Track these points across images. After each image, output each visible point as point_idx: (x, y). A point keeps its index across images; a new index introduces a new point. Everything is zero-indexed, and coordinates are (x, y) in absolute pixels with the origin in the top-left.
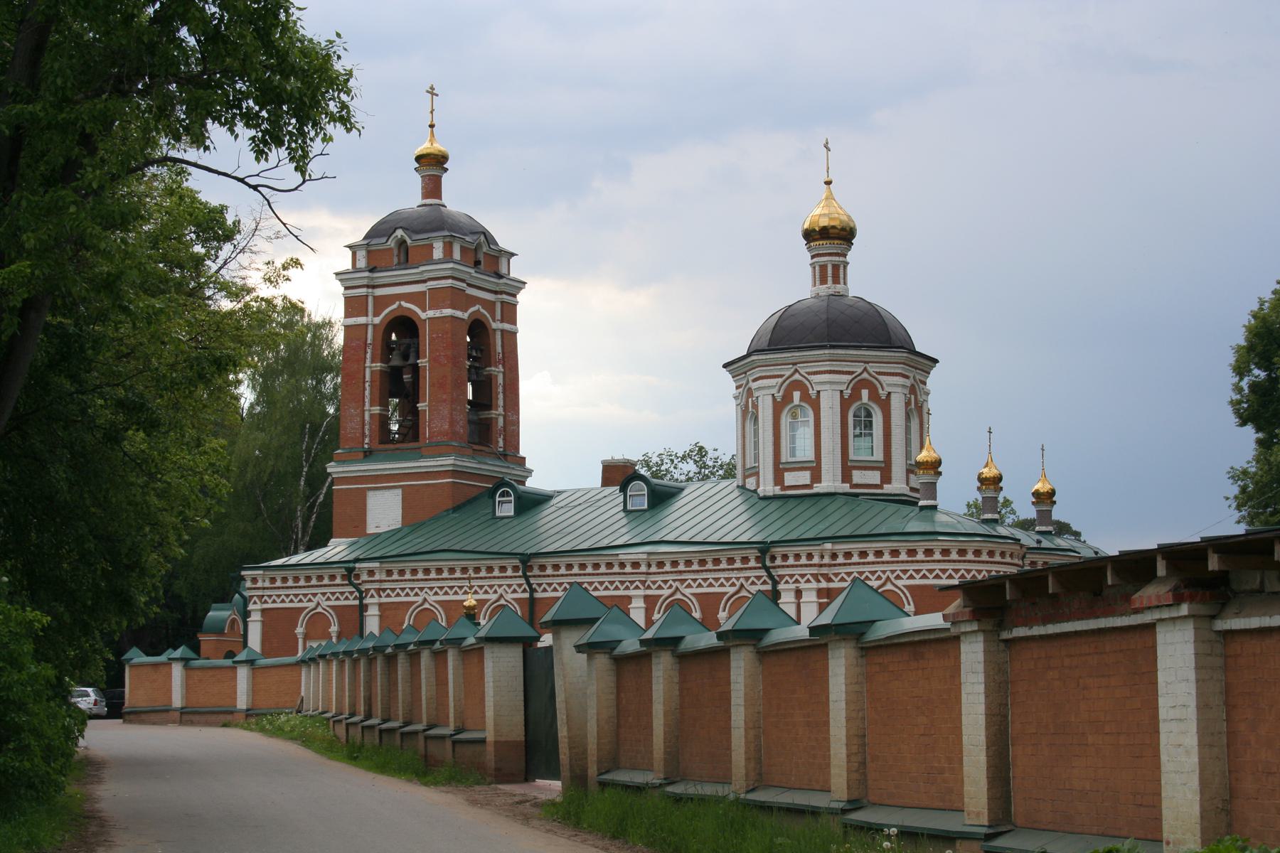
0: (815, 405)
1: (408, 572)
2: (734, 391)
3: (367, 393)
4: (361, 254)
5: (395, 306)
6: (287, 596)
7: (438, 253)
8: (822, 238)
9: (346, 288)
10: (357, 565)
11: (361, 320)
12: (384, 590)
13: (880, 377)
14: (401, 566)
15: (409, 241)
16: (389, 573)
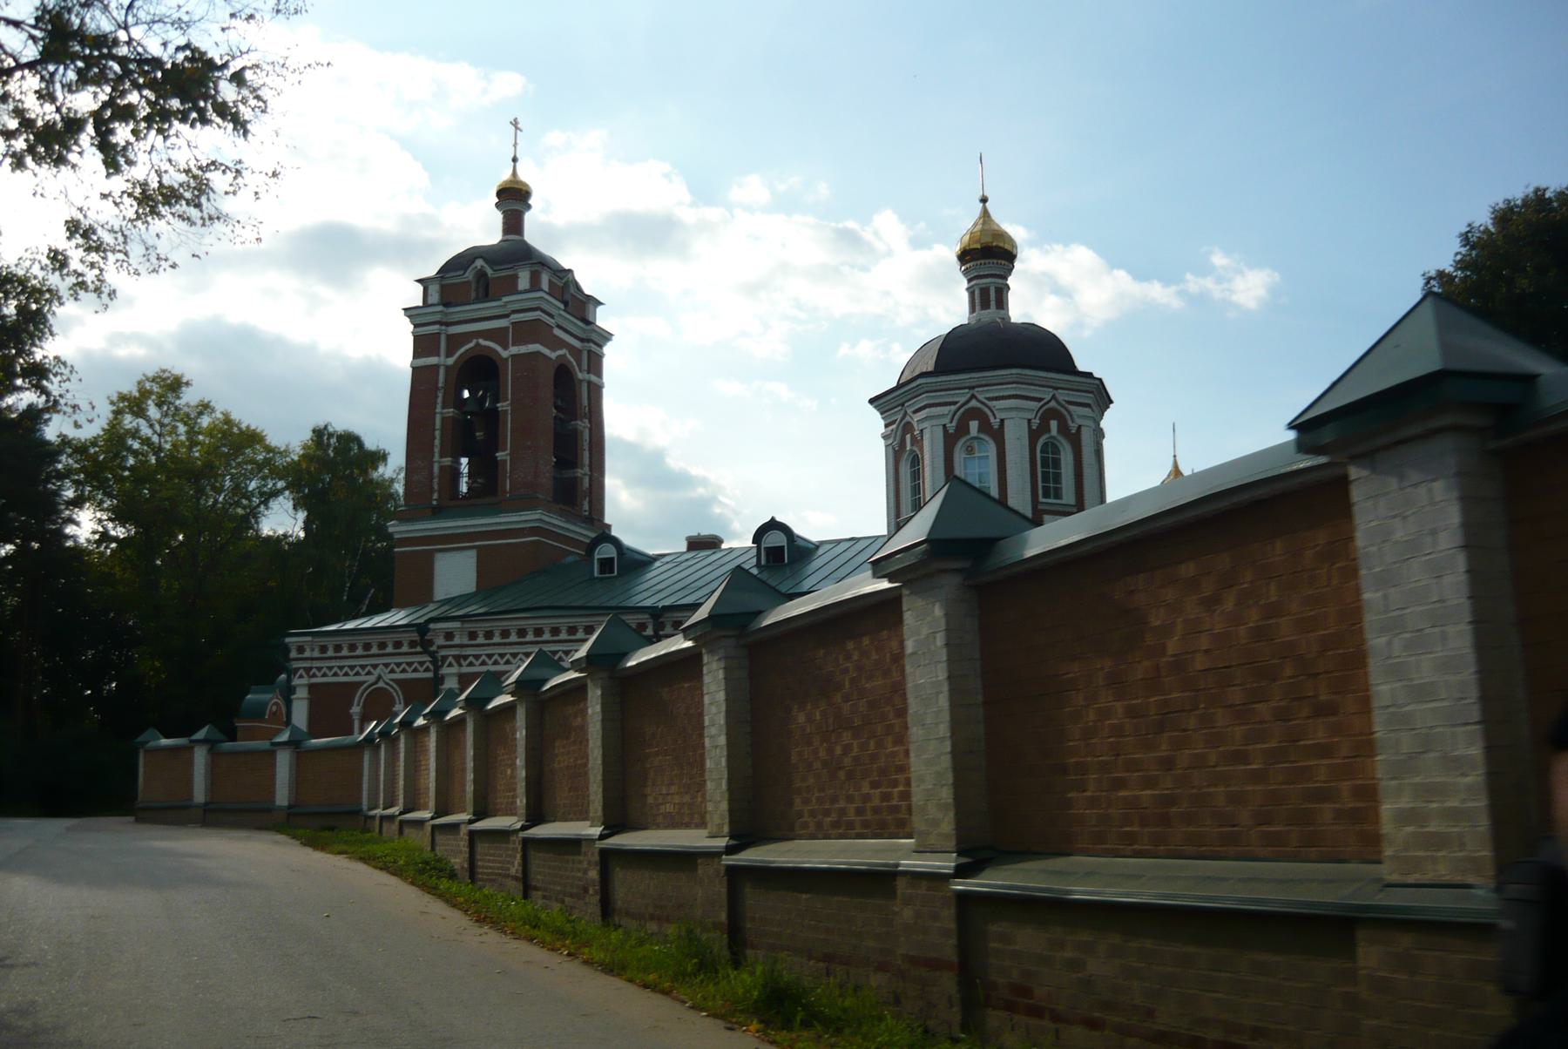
0: (998, 436)
1: (497, 634)
2: (883, 430)
3: (437, 442)
4: (434, 290)
5: (471, 345)
7: (524, 282)
8: (984, 257)
10: (432, 626)
11: (433, 360)
12: (465, 657)
13: (1071, 408)
15: (489, 272)
16: (473, 635)
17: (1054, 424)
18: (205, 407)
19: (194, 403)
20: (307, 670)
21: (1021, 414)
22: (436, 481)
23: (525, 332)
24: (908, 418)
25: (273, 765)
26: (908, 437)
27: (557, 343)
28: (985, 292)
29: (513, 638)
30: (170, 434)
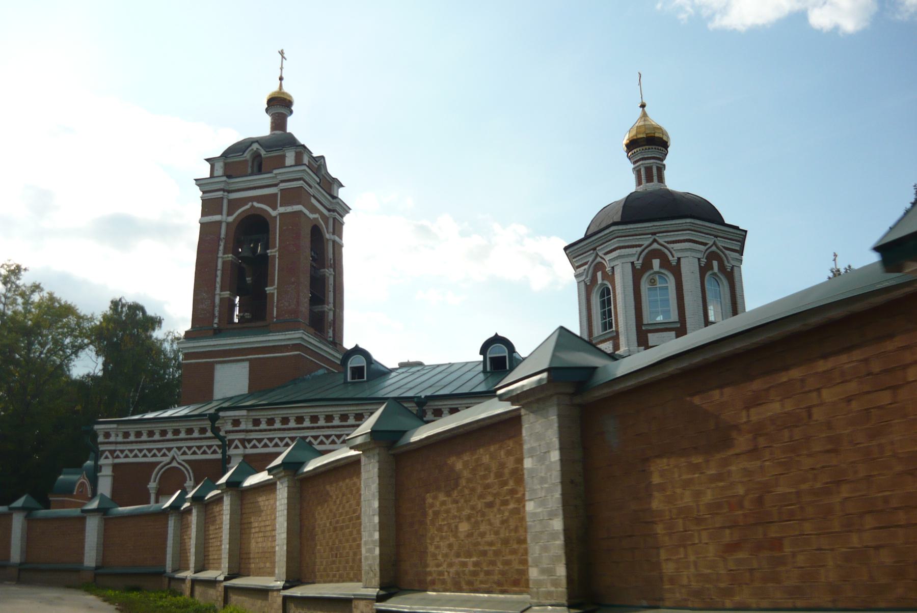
0: (676, 271)
1: (278, 421)
3: (218, 279)
5: (247, 207)
6: (140, 450)
7: (290, 159)
9: (204, 192)
10: (221, 414)
11: (217, 218)
12: (250, 441)
13: (727, 252)
14: (270, 414)
15: (263, 152)
16: (256, 422)
17: (715, 264)
18: (36, 288)
19: (29, 284)
20: (112, 452)
21: (694, 254)
22: (217, 309)
23: (291, 196)
24: (599, 259)
25: (82, 530)
26: (599, 274)
27: (314, 210)
28: (649, 170)
29: (292, 424)
30: (12, 304)
